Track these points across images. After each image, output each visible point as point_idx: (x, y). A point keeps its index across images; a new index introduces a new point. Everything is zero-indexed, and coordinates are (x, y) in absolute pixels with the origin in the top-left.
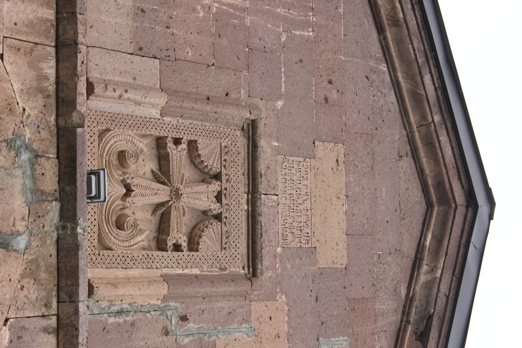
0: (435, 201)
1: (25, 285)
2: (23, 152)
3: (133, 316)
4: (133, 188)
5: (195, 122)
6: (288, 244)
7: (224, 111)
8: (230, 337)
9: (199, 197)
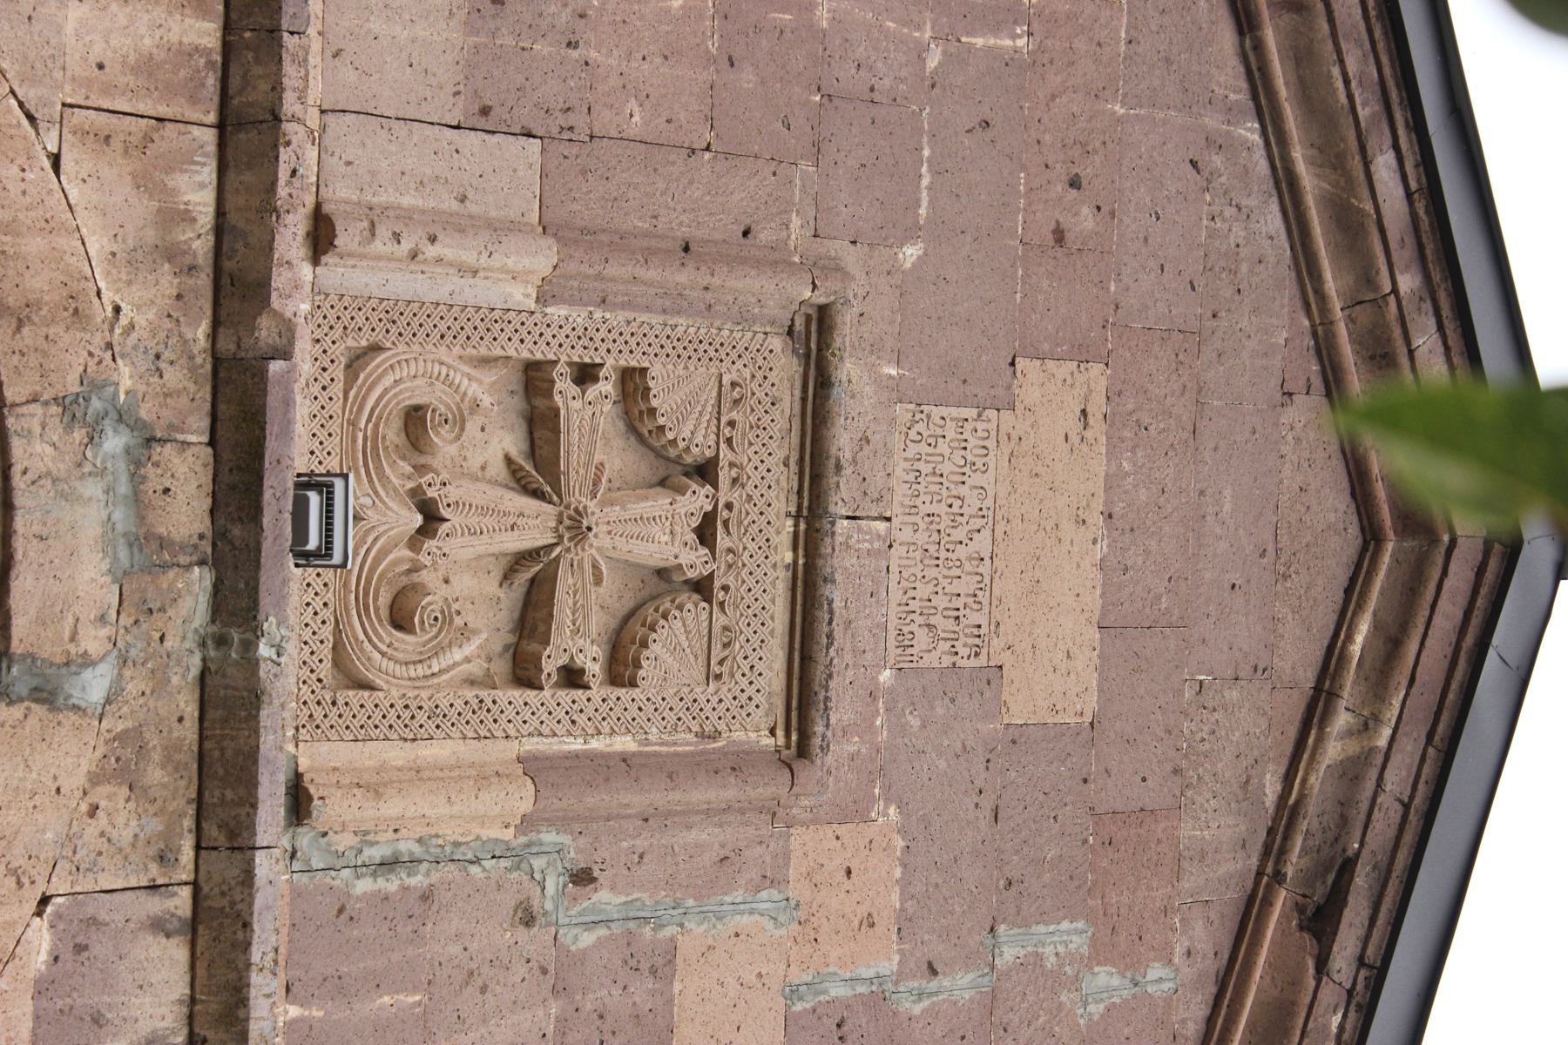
0: (1388, 523)
1: (103, 804)
2: (109, 431)
4: (444, 513)
6: (915, 658)
7: (732, 283)
8: (719, 926)
9: (656, 530)
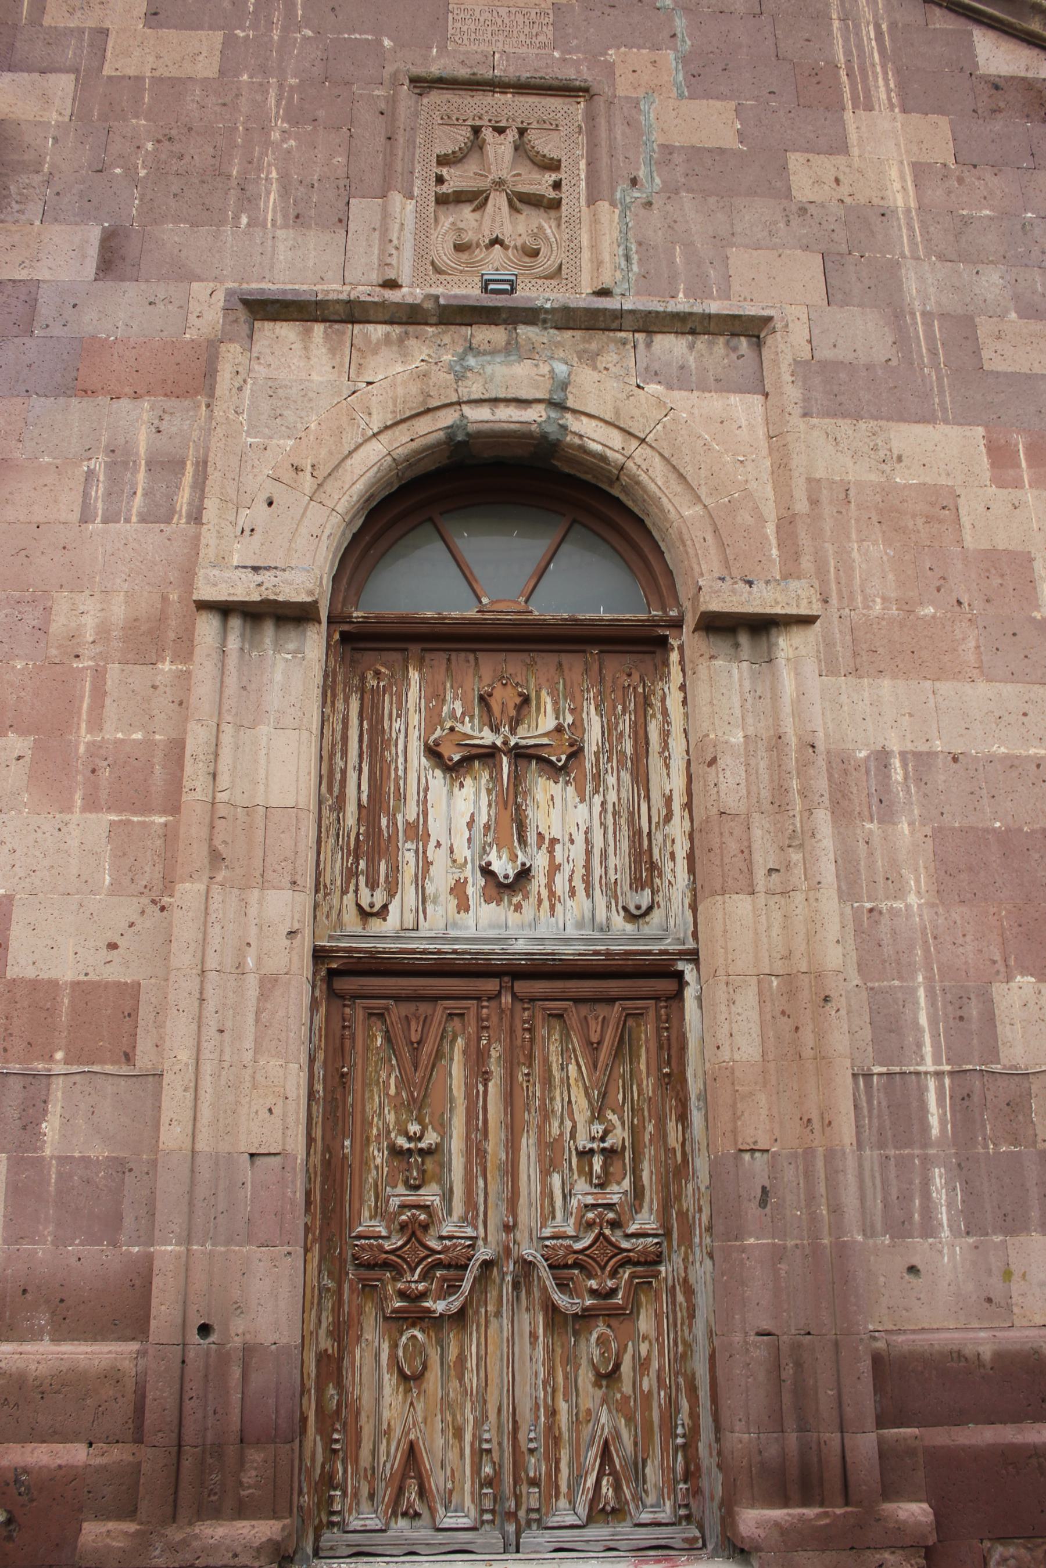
4: (494, 236)
7: (402, 119)
9: (500, 150)
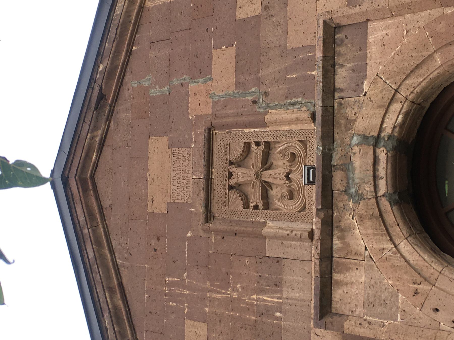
0: (89, 180)
1: (353, 115)
2: (354, 193)
3: (287, 102)
5: (244, 219)
7: (226, 227)
9: (241, 175)
